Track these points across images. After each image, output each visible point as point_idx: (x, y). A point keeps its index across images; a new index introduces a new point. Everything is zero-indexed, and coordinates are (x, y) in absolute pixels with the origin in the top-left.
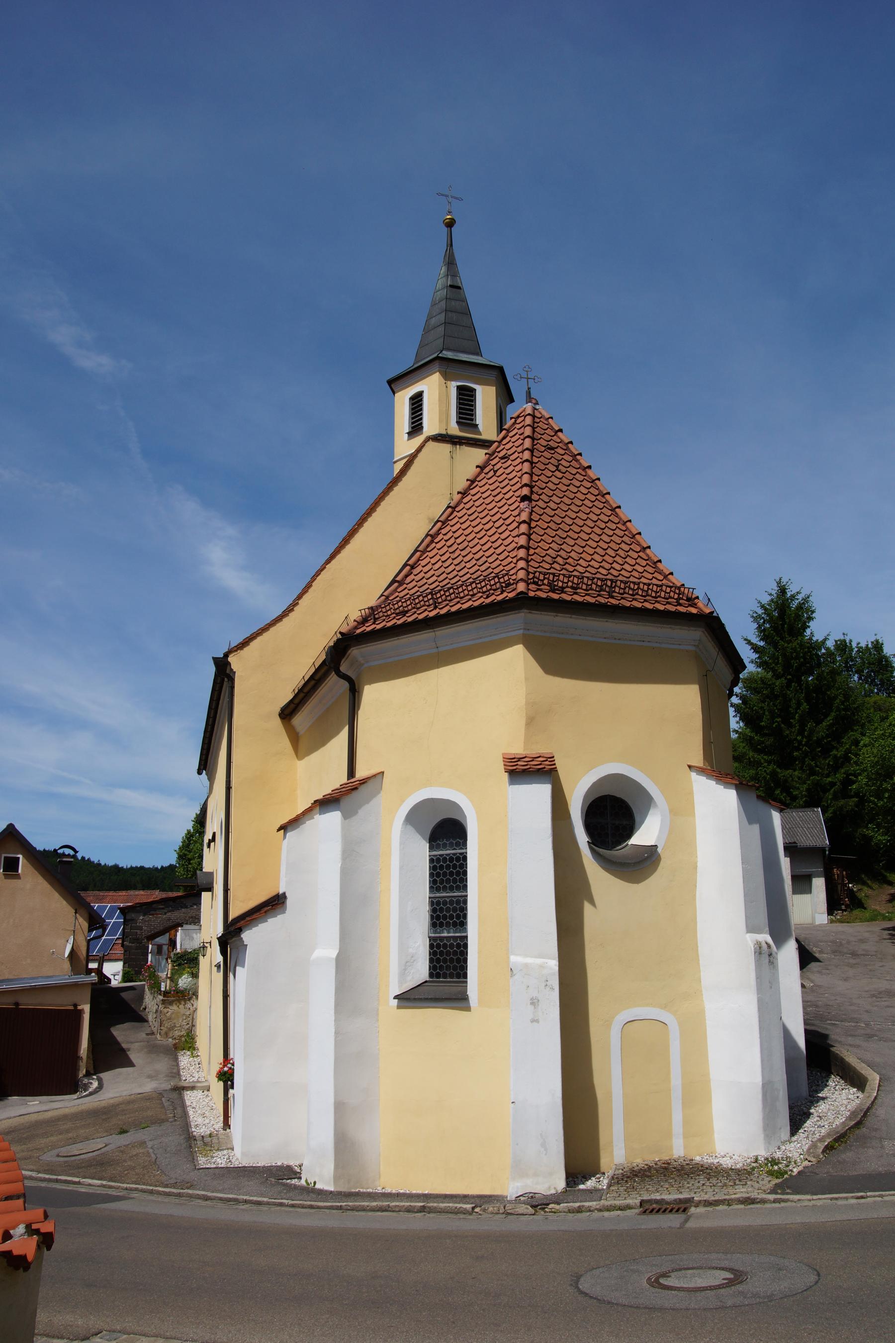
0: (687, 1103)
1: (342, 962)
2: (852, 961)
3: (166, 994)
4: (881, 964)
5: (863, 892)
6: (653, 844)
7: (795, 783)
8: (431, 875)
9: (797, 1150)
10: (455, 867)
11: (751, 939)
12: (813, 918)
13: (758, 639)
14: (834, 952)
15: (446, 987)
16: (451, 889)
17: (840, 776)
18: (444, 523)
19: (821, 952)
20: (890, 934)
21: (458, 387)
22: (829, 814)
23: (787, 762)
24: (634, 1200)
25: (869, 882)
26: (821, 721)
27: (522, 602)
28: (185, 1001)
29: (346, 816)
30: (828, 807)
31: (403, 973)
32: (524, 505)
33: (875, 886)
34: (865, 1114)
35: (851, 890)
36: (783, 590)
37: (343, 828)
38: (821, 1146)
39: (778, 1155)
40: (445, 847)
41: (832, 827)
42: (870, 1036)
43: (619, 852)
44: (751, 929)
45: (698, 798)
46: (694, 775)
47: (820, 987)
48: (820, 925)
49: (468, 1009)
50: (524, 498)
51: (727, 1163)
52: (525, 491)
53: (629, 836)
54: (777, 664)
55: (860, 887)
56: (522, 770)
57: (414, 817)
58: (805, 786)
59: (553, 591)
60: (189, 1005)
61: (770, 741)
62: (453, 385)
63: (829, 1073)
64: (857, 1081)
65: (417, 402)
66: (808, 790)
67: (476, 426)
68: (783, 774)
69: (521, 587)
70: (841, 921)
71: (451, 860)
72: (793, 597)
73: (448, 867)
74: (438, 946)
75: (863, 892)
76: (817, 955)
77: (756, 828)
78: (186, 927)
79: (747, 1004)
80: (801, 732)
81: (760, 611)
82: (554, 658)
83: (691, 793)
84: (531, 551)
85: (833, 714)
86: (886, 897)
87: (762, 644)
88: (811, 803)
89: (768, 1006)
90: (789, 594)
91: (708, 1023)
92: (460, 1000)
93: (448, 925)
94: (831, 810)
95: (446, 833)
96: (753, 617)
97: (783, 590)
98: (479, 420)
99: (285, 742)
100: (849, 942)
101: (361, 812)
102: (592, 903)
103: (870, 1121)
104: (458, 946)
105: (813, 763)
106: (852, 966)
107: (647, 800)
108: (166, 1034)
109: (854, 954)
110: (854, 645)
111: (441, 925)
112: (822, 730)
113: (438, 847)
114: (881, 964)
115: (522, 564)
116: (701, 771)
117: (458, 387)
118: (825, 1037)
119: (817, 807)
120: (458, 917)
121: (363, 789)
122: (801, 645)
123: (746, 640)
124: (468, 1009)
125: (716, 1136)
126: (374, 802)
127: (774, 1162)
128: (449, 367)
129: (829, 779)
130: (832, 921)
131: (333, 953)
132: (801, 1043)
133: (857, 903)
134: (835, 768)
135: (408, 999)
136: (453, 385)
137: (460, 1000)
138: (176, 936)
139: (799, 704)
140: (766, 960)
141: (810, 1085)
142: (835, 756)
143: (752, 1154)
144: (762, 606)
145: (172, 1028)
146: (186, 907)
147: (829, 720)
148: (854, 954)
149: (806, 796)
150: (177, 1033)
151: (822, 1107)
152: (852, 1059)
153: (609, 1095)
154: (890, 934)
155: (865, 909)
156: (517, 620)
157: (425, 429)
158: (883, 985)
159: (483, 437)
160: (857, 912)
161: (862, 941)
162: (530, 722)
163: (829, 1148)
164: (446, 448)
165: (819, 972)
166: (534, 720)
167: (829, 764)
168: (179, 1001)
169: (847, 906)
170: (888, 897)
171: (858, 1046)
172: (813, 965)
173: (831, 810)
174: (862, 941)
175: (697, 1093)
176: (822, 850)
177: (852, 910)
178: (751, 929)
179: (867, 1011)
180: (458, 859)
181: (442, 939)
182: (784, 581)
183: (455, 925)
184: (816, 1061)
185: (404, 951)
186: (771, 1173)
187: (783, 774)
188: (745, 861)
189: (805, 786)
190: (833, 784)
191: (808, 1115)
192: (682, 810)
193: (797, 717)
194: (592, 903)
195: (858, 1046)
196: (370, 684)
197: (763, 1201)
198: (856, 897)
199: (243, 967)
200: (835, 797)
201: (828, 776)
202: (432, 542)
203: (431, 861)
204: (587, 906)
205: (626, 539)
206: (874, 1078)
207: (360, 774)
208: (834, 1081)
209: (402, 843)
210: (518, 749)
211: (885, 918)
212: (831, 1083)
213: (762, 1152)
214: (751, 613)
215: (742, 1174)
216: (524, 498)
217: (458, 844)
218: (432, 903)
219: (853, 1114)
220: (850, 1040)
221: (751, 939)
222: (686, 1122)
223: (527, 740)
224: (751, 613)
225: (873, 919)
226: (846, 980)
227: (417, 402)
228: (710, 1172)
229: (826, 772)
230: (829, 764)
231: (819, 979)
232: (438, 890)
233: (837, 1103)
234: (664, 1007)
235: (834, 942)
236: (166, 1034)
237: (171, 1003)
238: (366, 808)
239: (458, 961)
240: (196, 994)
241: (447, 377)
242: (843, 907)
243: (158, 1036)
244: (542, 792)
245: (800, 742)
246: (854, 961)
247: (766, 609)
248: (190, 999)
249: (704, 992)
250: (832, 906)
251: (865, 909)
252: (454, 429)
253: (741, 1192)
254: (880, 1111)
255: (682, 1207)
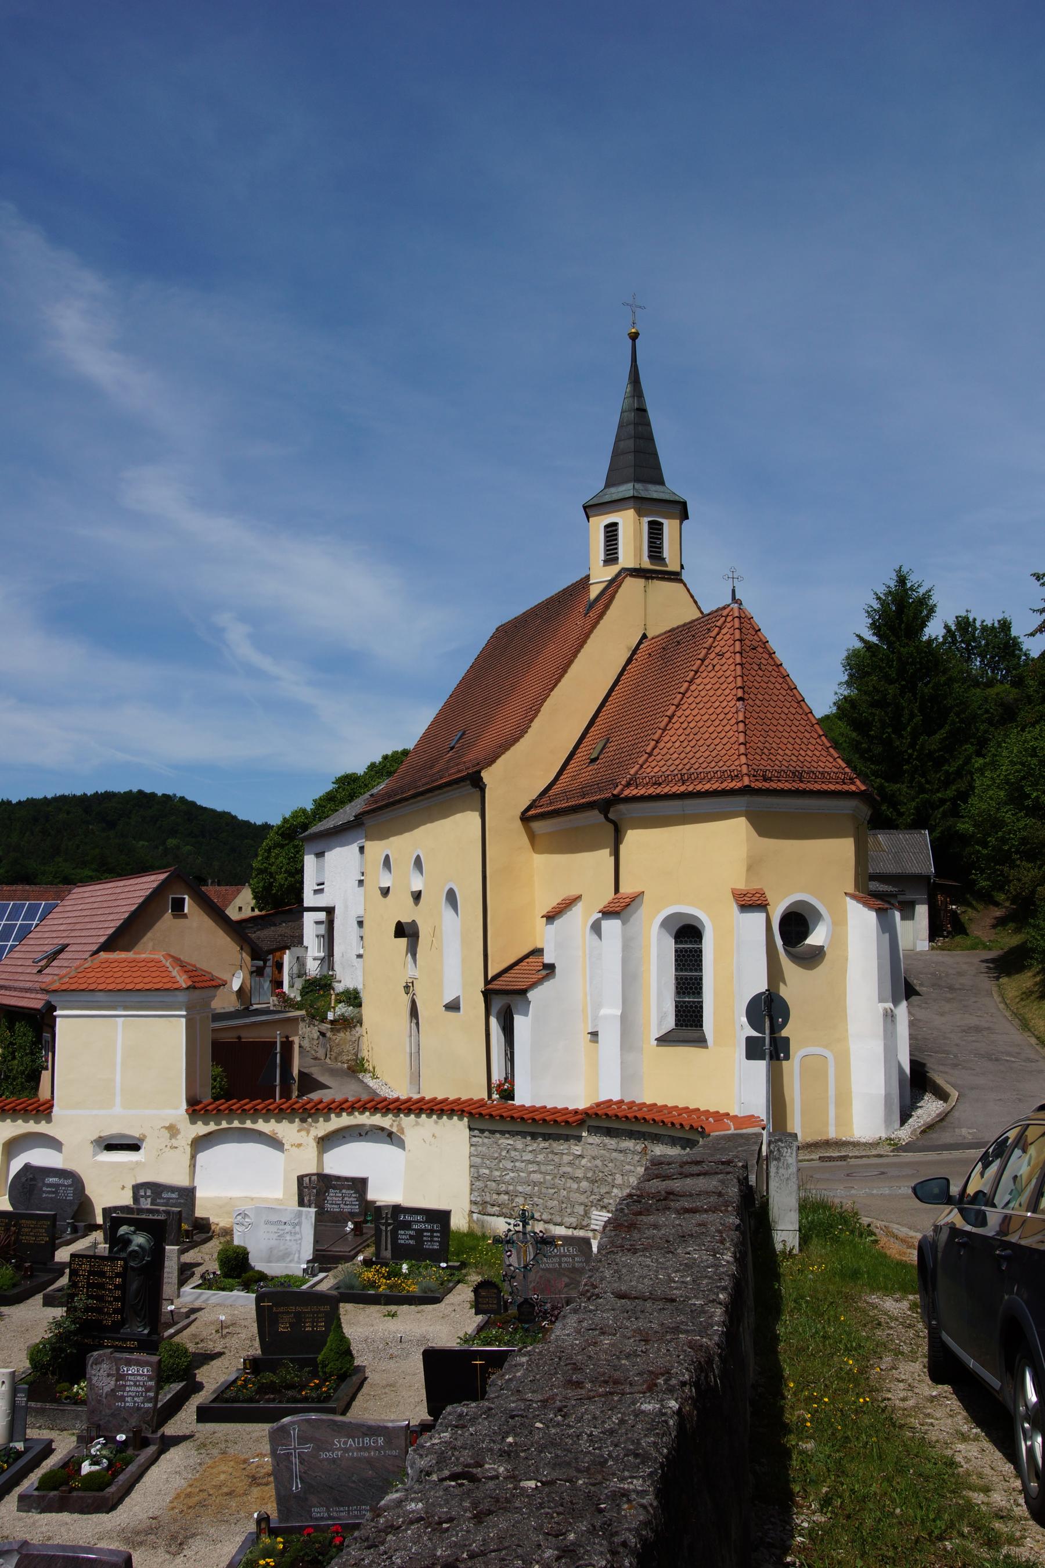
0: (838, 1105)
1: (624, 1018)
2: (949, 995)
3: (332, 1022)
4: (974, 999)
5: (967, 915)
6: (821, 944)
7: (902, 798)
8: (676, 960)
9: (904, 1134)
10: (693, 956)
11: (881, 1006)
12: (915, 944)
13: (871, 632)
14: (933, 985)
15: (691, 1033)
16: (691, 970)
17: (950, 793)
18: (677, 706)
19: (921, 985)
20: (988, 967)
21: (650, 523)
22: (936, 834)
23: (894, 776)
24: (815, 1156)
25: (974, 902)
26: (935, 733)
27: (746, 791)
28: (351, 1028)
29: (624, 923)
30: (935, 826)
31: (660, 1024)
32: (740, 704)
33: (980, 907)
34: (946, 1115)
35: (954, 912)
36: (902, 580)
37: (622, 931)
38: (919, 1131)
39: (893, 1136)
40: (686, 942)
41: (939, 850)
42: (955, 1066)
43: (799, 949)
44: (881, 1000)
45: (850, 915)
46: (848, 899)
47: (919, 1020)
48: (921, 953)
49: (707, 1047)
50: (740, 699)
51: (863, 1140)
52: (740, 693)
53: (805, 938)
54: (890, 667)
55: (963, 909)
56: (751, 902)
57: (666, 923)
58: (914, 804)
59: (765, 780)
60: (354, 1032)
61: (878, 750)
62: (646, 520)
63: (925, 1091)
64: (943, 1096)
65: (611, 531)
66: (916, 808)
67: (664, 559)
68: (892, 787)
69: (746, 781)
70: (942, 949)
71: (691, 951)
72: (911, 589)
73: (689, 956)
74: (682, 1007)
75: (967, 915)
76: (917, 988)
77: (887, 935)
78: (293, 949)
79: (877, 1047)
80: (912, 745)
81: (876, 605)
82: (766, 826)
83: (845, 911)
84: (748, 745)
85: (947, 727)
86: (989, 921)
87: (874, 639)
88: (918, 824)
89: (890, 1050)
90: (909, 585)
91: (852, 1058)
92: (701, 1041)
93: (689, 993)
94: (939, 830)
95: (687, 935)
96: (868, 612)
97: (902, 580)
98: (666, 554)
99: (525, 840)
100: (947, 975)
101: (632, 920)
102: (785, 984)
103: (947, 1119)
104: (696, 1007)
105: (923, 780)
106: (949, 1001)
107: (818, 916)
108: (336, 1058)
109: (951, 988)
110: (978, 624)
111: (684, 993)
112: (934, 742)
113: (681, 942)
114: (974, 999)
115: (743, 759)
116: (853, 897)
117: (650, 523)
118: (924, 1065)
119: (925, 829)
120: (696, 988)
121: (633, 904)
122: (917, 648)
123: (858, 636)
124: (707, 1047)
125: (855, 1126)
126: (639, 911)
127: (891, 1139)
128: (641, 504)
129: (939, 795)
130: (932, 948)
131: (618, 1012)
132: (908, 1070)
133: (960, 928)
134: (946, 784)
135: (665, 1041)
136: (646, 520)
137: (701, 1041)
138: (282, 958)
139: (912, 716)
140: (889, 1019)
141: (912, 1098)
142: (947, 772)
143: (877, 1136)
144: (879, 598)
145: (340, 1053)
146: (275, 925)
147: (942, 734)
148: (951, 988)
149: (913, 814)
150: (345, 1058)
151: (919, 1111)
152: (940, 1081)
153: (793, 1099)
154: (988, 967)
155: (967, 935)
156: (742, 801)
157: (620, 560)
158: (973, 1021)
159: (669, 569)
160: (958, 939)
161: (960, 974)
162: (750, 868)
163: (923, 1132)
164: (640, 582)
165: (919, 1006)
166: (753, 866)
167: (939, 779)
168: (345, 1028)
169: (949, 932)
170: (993, 921)
171: (946, 1073)
172: (914, 998)
173: (939, 830)
174: (960, 974)
175: (844, 1100)
176: (928, 877)
177: (953, 937)
178: (881, 1000)
179: (957, 1045)
180: (696, 951)
181: (684, 1002)
182: (905, 570)
183: (694, 993)
184: (917, 1082)
185: (659, 1009)
186: (890, 1144)
187: (892, 787)
188: (879, 958)
189: (914, 804)
190: (942, 801)
191: (911, 1116)
192: (839, 922)
193: (909, 729)
194: (785, 984)
195: (946, 1073)
196: (632, 828)
197: (887, 1156)
198: (959, 921)
199: (526, 1014)
200: (944, 815)
201: (938, 791)
202: (670, 722)
203: (676, 951)
204: (782, 985)
205: (808, 728)
206: (955, 1094)
207: (626, 889)
208: (927, 1097)
209: (659, 940)
210: (741, 885)
211: (986, 947)
212: (926, 1098)
213: (884, 1136)
214: (866, 607)
215: (875, 1144)
216: (740, 699)
217: (696, 942)
218: (677, 979)
219: (939, 1115)
220: (942, 1068)
221: (881, 1006)
222: (837, 1117)
223: (747, 881)
224: (866, 607)
225: (973, 948)
226: (942, 1014)
227: (611, 531)
228: (856, 1144)
229: (936, 787)
230: (939, 779)
231: (921, 1014)
232: (681, 970)
233: (930, 1108)
234: (826, 1047)
235: (933, 974)
236: (336, 1058)
237: (338, 1031)
238: (635, 916)
239: (696, 1016)
240: (360, 1022)
241: (640, 513)
242: (945, 933)
243: (328, 1061)
244: (759, 918)
245: (910, 755)
246: (949, 995)
247: (879, 598)
248: (355, 1027)
249: (850, 1039)
250: (934, 932)
251: (967, 935)
252: (646, 563)
253: (874, 1152)
254: (956, 1114)
255: (843, 1158)
